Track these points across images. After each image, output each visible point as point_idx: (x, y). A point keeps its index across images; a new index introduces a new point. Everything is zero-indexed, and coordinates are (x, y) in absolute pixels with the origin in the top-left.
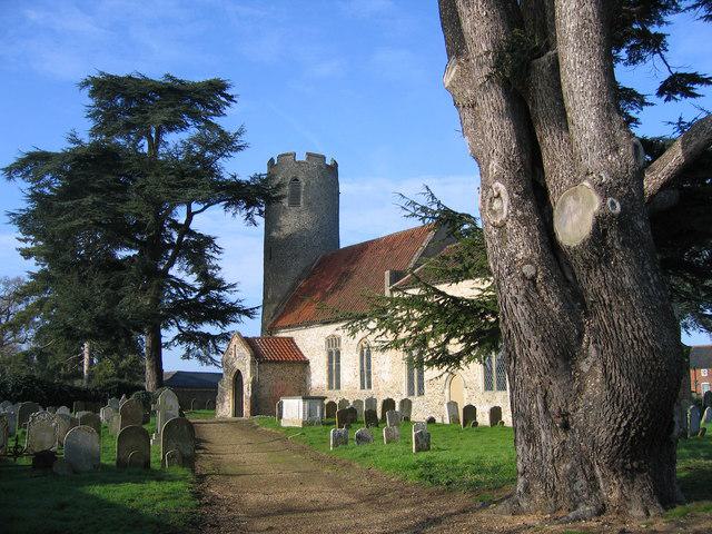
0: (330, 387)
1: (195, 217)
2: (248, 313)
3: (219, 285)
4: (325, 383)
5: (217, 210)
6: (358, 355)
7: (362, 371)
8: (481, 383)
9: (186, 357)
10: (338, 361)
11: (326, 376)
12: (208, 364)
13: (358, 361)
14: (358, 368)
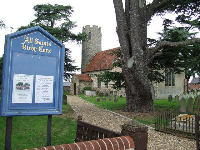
11: (97, 85)
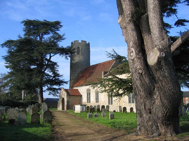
0: (88, 102)
1: (52, 57)
2: (66, 83)
3: (58, 75)
4: (86, 101)
5: (58, 55)
6: (95, 94)
7: (96, 98)
8: (128, 101)
9: (49, 94)
10: (90, 95)
11: (86, 99)
12: (55, 96)
13: (95, 95)
14: (95, 97)
